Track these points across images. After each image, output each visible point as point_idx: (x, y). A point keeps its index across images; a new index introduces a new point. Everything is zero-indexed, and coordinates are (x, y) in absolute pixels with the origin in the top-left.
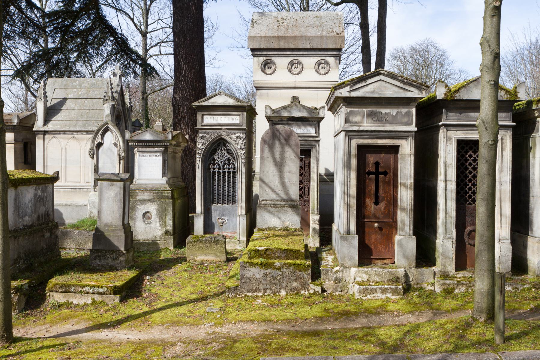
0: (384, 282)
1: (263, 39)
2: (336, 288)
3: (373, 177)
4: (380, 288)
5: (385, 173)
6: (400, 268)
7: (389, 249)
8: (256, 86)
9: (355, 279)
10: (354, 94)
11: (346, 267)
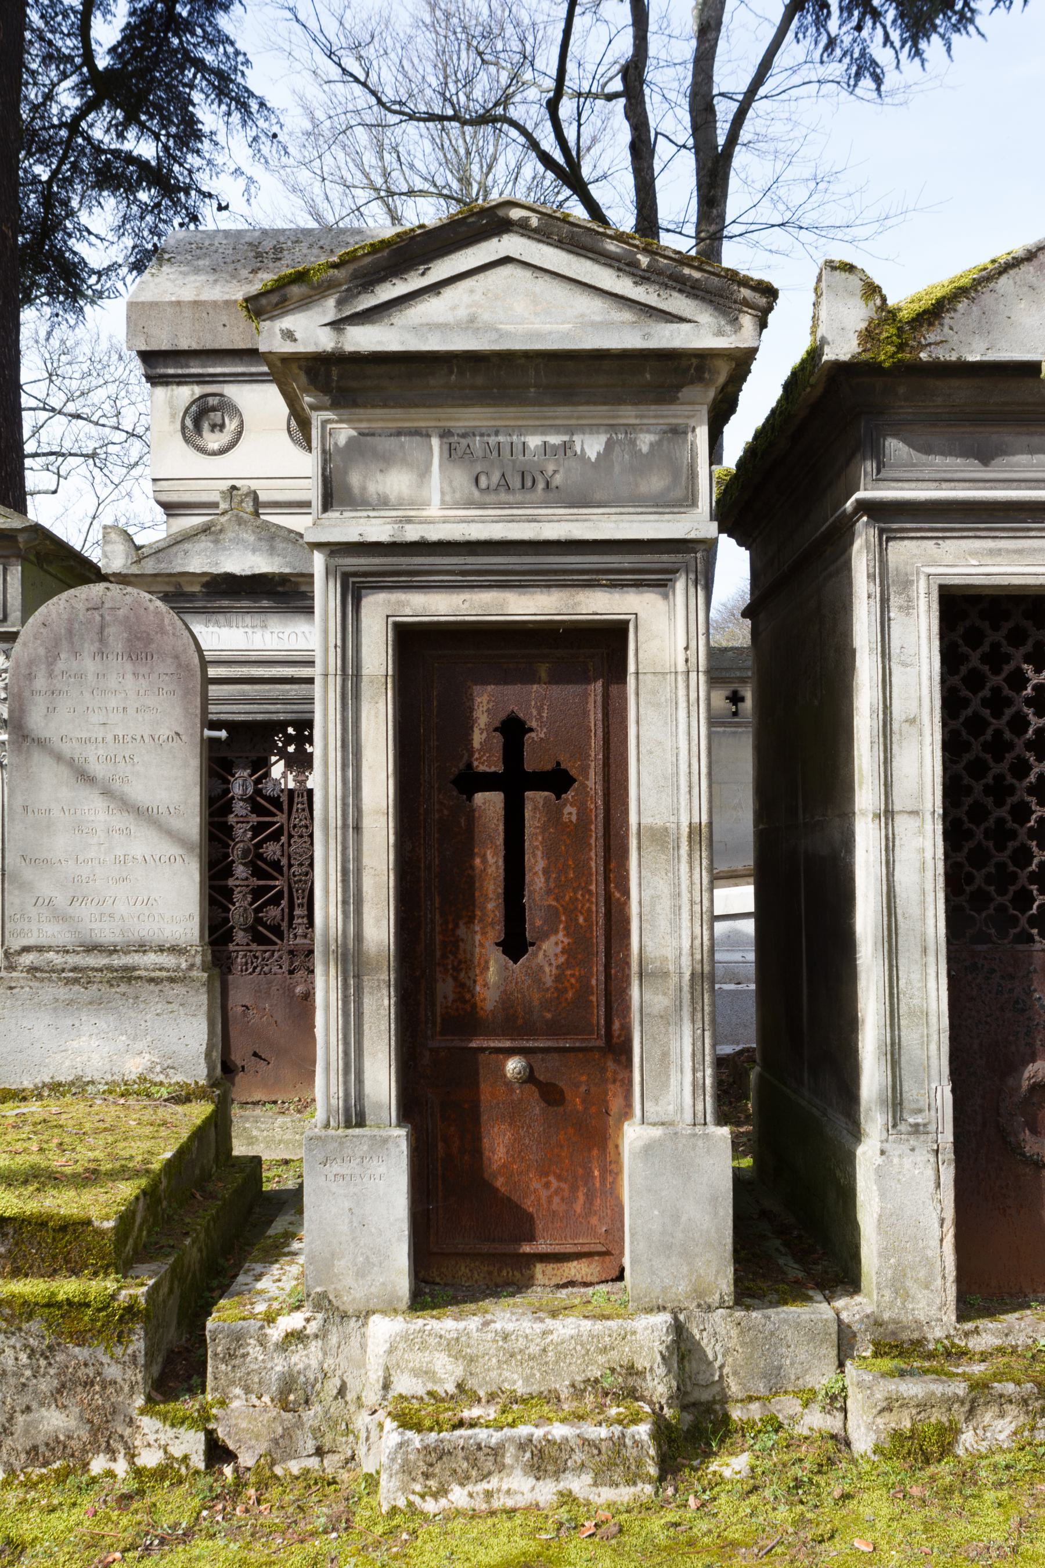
0: (552, 1398)
1: (188, 313)
2: (287, 1433)
4: (523, 1445)
6: (649, 1310)
7: (590, 1198)
8: (165, 498)
9: (386, 1387)
10: (364, 339)
11: (344, 1316)
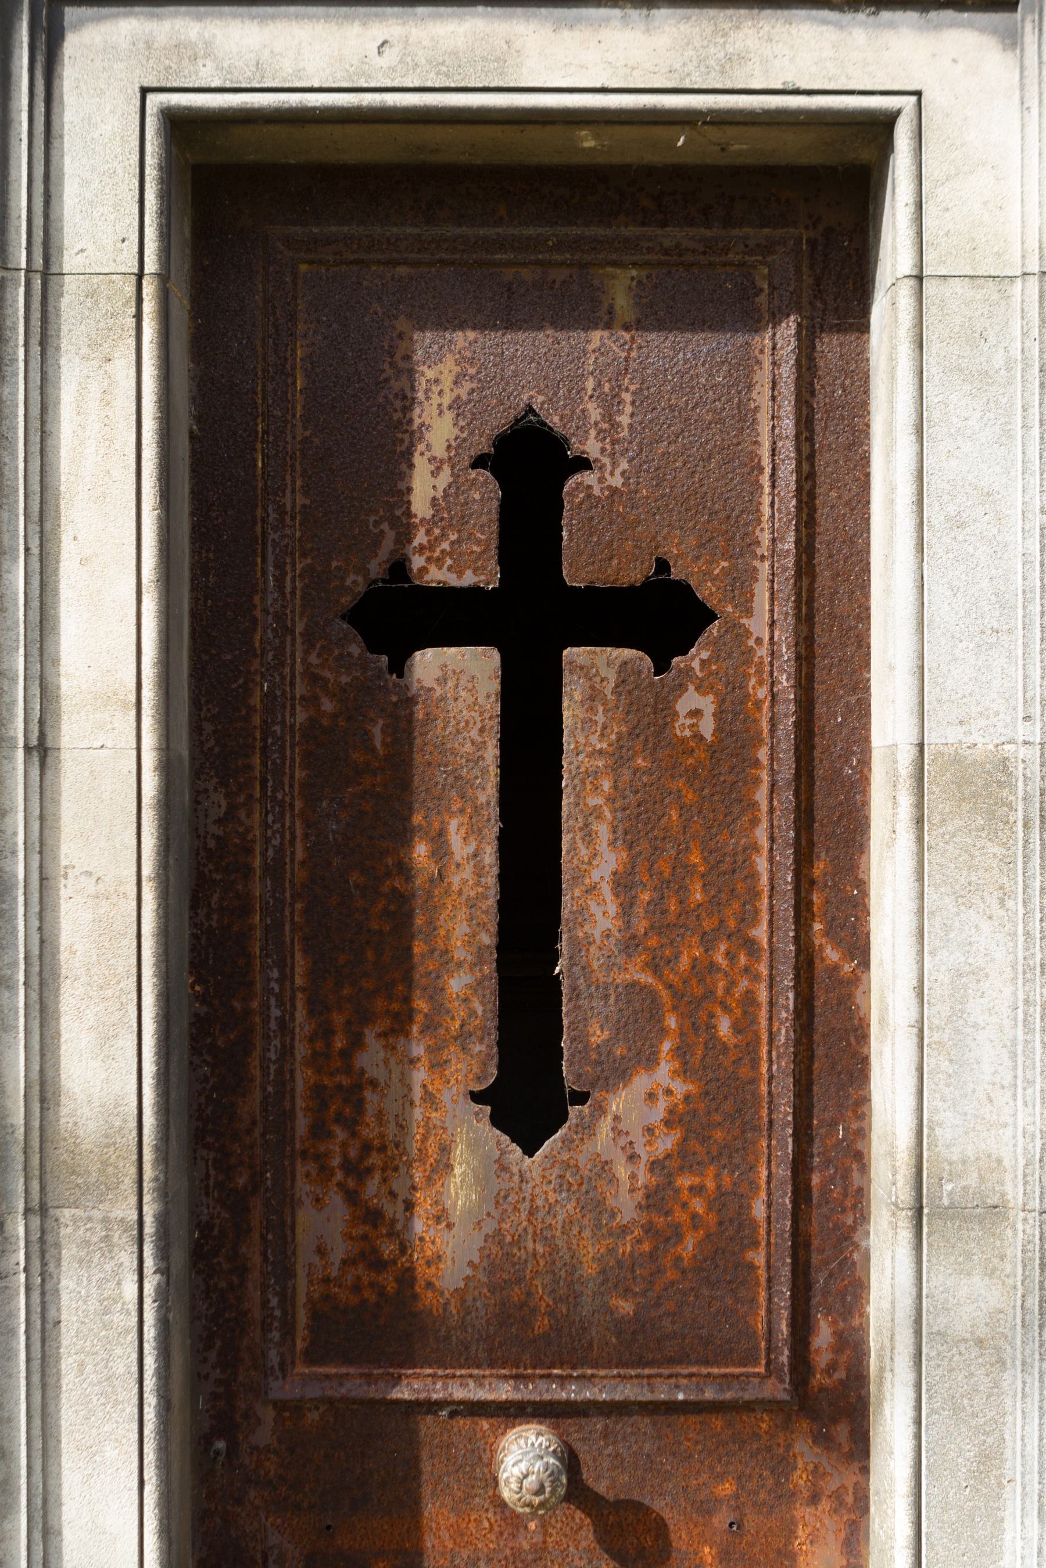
3: (459, 681)
5: (663, 617)
